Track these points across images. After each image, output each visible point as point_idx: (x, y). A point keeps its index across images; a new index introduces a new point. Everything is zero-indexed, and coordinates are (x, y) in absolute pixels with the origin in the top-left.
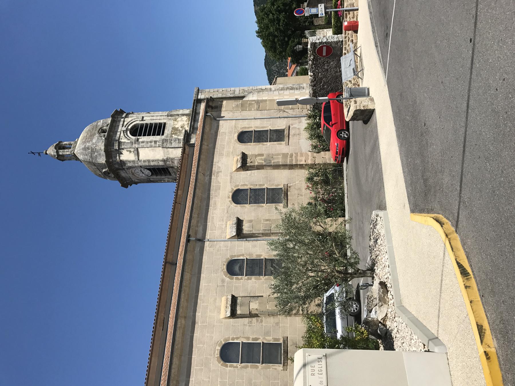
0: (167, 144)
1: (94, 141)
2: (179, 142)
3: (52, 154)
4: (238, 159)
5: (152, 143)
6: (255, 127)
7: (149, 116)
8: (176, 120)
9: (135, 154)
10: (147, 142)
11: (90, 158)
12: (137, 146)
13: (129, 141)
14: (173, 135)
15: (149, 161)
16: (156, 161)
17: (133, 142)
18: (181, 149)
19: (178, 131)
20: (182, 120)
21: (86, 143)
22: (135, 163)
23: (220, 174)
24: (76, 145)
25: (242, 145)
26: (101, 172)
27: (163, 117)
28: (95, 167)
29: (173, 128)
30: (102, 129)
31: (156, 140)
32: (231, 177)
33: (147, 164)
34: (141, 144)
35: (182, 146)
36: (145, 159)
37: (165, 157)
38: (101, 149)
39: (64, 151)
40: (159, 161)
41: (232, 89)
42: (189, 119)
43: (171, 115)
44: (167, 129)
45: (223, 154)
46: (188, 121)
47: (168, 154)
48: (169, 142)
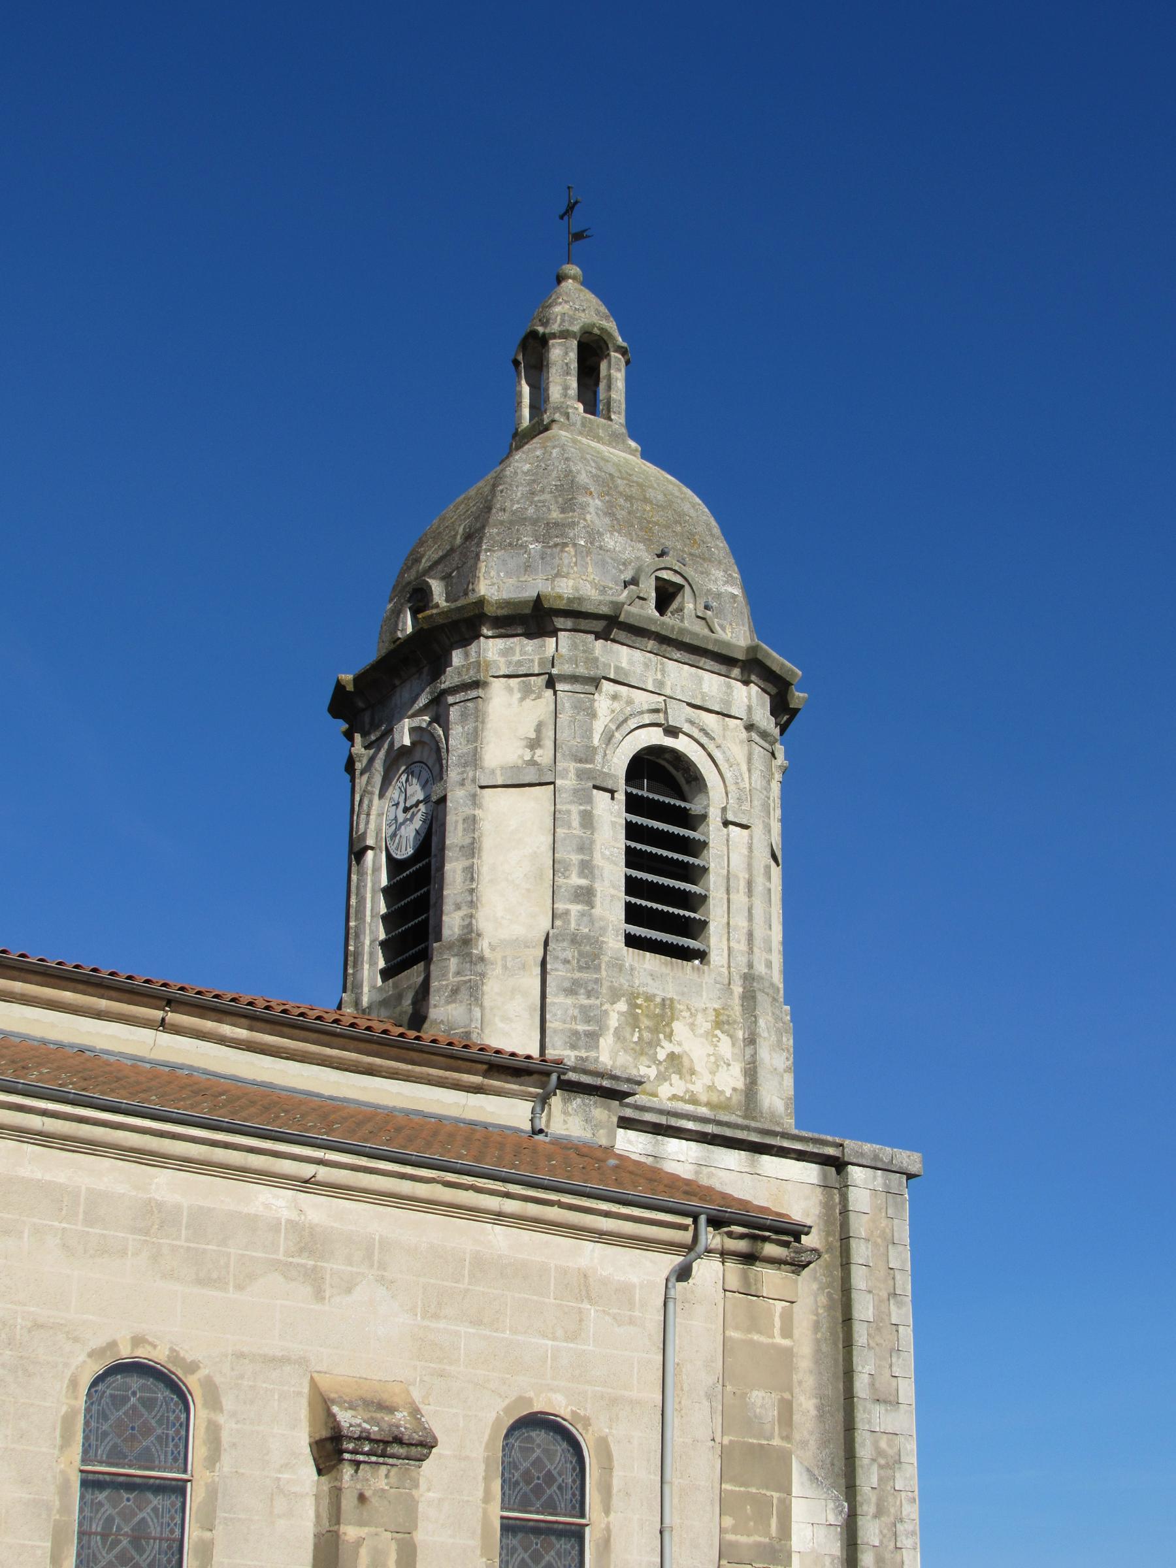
0: (566, 961)
1: (613, 541)
2: (574, 1039)
3: (557, 309)
4: (391, 1410)
5: (581, 874)
6: (608, 1529)
7: (750, 867)
8: (718, 1024)
9: (515, 768)
10: (585, 847)
11: (514, 513)
12: (566, 782)
13: (596, 742)
14: (622, 1006)
15: (472, 850)
16: (472, 891)
17: (590, 760)
18: (535, 1052)
19: (647, 1035)
20: (718, 1063)
21: (600, 496)
22: (465, 765)
23: (307, 1290)
24: (599, 439)
25: (492, 1439)
26: (428, 571)
27: (740, 946)
28: (459, 540)
29: (672, 1008)
30: (681, 587)
31: (598, 900)
32: (273, 1359)
33: (455, 836)
34: (575, 809)
35: (551, 1053)
36: (486, 826)
37: (493, 948)
38: (558, 575)
39: (568, 374)
40: (464, 911)
41: (907, 1391)
42: (725, 1106)
43: (754, 998)
44: (665, 970)
45: (436, 1316)
46: (715, 1098)
47: (505, 967)
48: (577, 975)
